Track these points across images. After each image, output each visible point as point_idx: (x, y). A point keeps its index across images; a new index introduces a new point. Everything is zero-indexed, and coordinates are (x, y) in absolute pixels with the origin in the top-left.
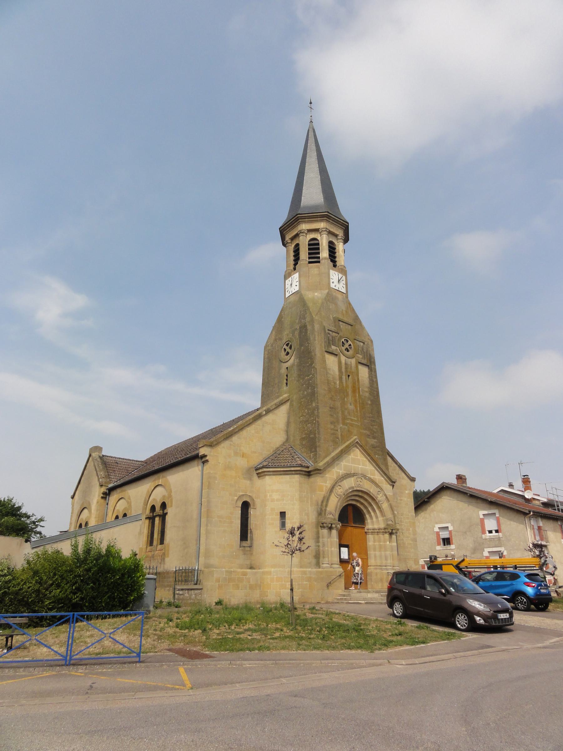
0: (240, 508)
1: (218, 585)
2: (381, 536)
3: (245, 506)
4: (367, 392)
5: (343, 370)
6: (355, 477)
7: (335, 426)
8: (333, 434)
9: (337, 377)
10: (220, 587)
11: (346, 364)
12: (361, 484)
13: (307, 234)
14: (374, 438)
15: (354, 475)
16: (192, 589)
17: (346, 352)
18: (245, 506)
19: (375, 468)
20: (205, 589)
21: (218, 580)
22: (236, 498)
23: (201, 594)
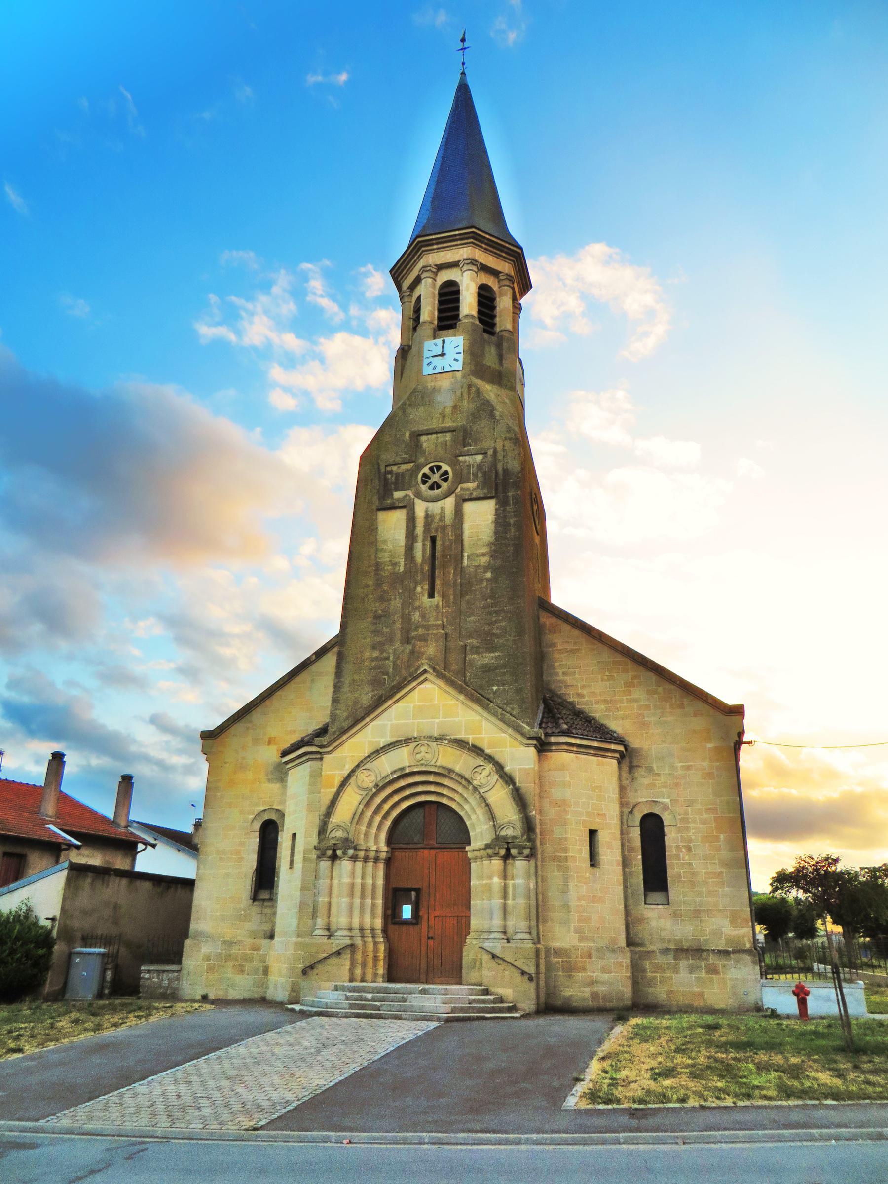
0: (258, 834)
1: (208, 965)
2: (486, 863)
3: (592, 833)
4: (483, 555)
5: (419, 530)
6: (413, 745)
7: (382, 652)
8: (377, 667)
9: (402, 551)
10: (211, 969)
11: (427, 516)
12: (428, 756)
13: (436, 274)
14: (491, 649)
15: (407, 741)
16: (164, 971)
17: (436, 492)
18: (592, 833)
19: (481, 715)
20: (184, 972)
21: (207, 958)
22: (252, 817)
23: (178, 979)
